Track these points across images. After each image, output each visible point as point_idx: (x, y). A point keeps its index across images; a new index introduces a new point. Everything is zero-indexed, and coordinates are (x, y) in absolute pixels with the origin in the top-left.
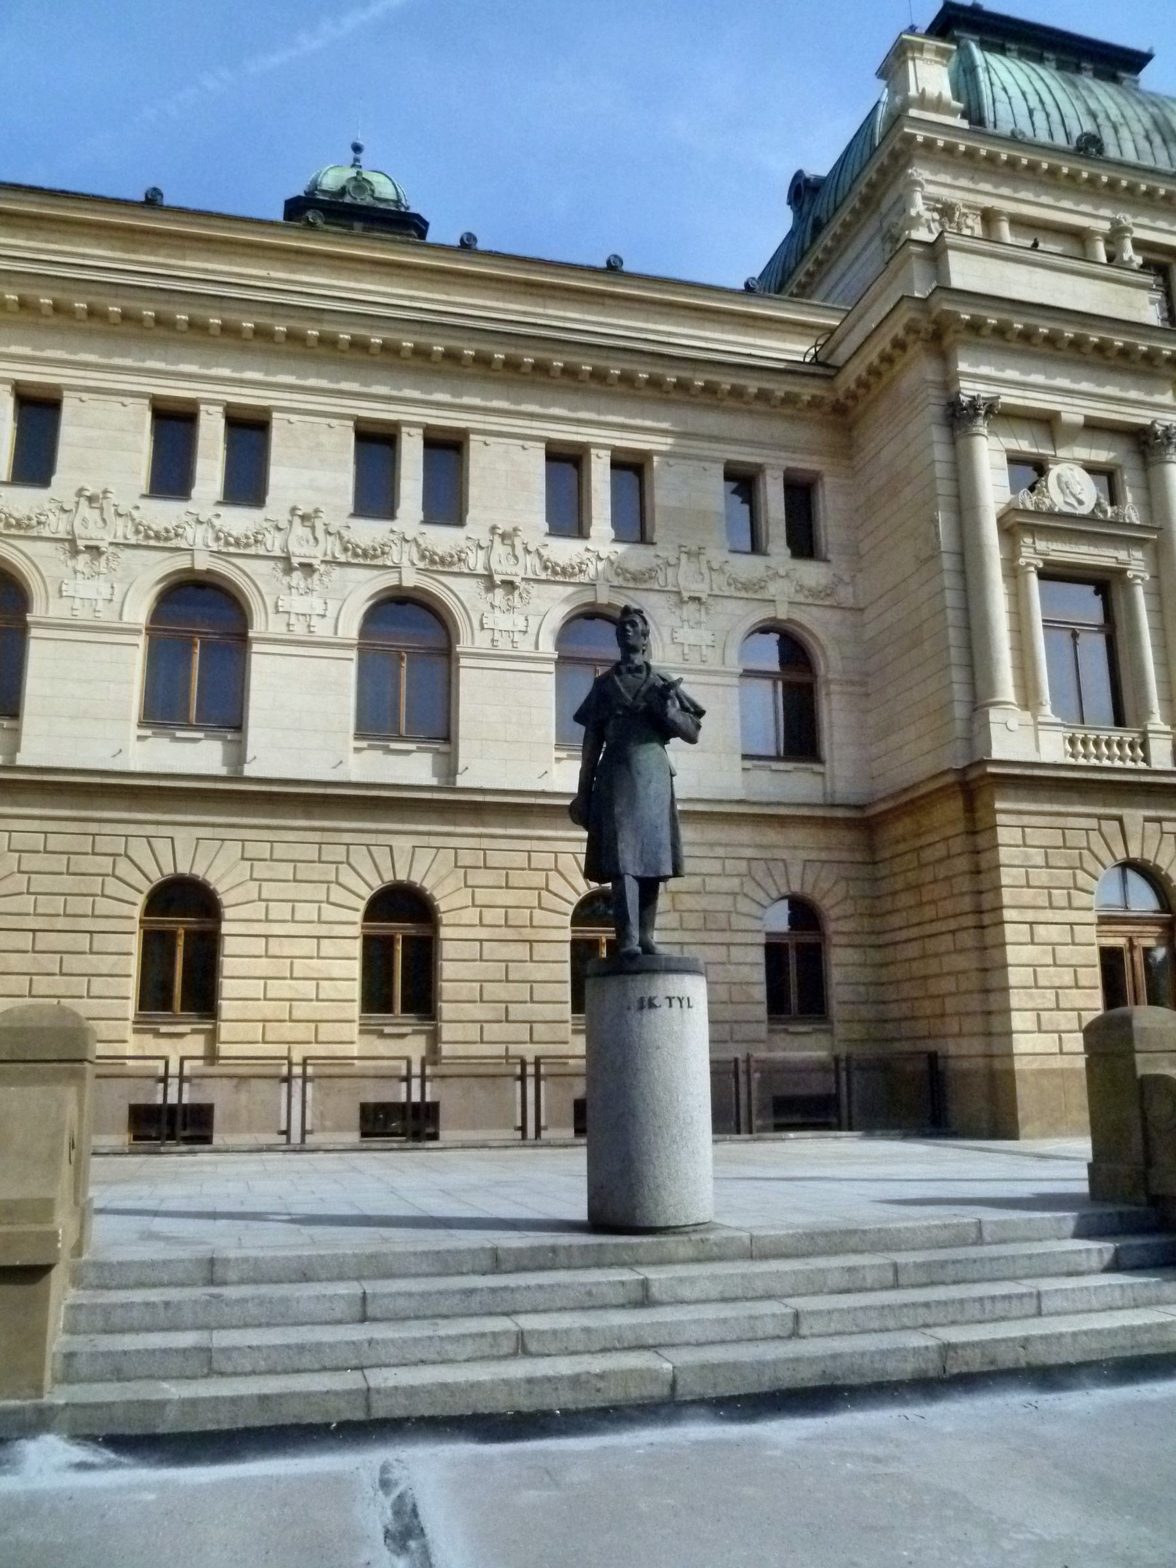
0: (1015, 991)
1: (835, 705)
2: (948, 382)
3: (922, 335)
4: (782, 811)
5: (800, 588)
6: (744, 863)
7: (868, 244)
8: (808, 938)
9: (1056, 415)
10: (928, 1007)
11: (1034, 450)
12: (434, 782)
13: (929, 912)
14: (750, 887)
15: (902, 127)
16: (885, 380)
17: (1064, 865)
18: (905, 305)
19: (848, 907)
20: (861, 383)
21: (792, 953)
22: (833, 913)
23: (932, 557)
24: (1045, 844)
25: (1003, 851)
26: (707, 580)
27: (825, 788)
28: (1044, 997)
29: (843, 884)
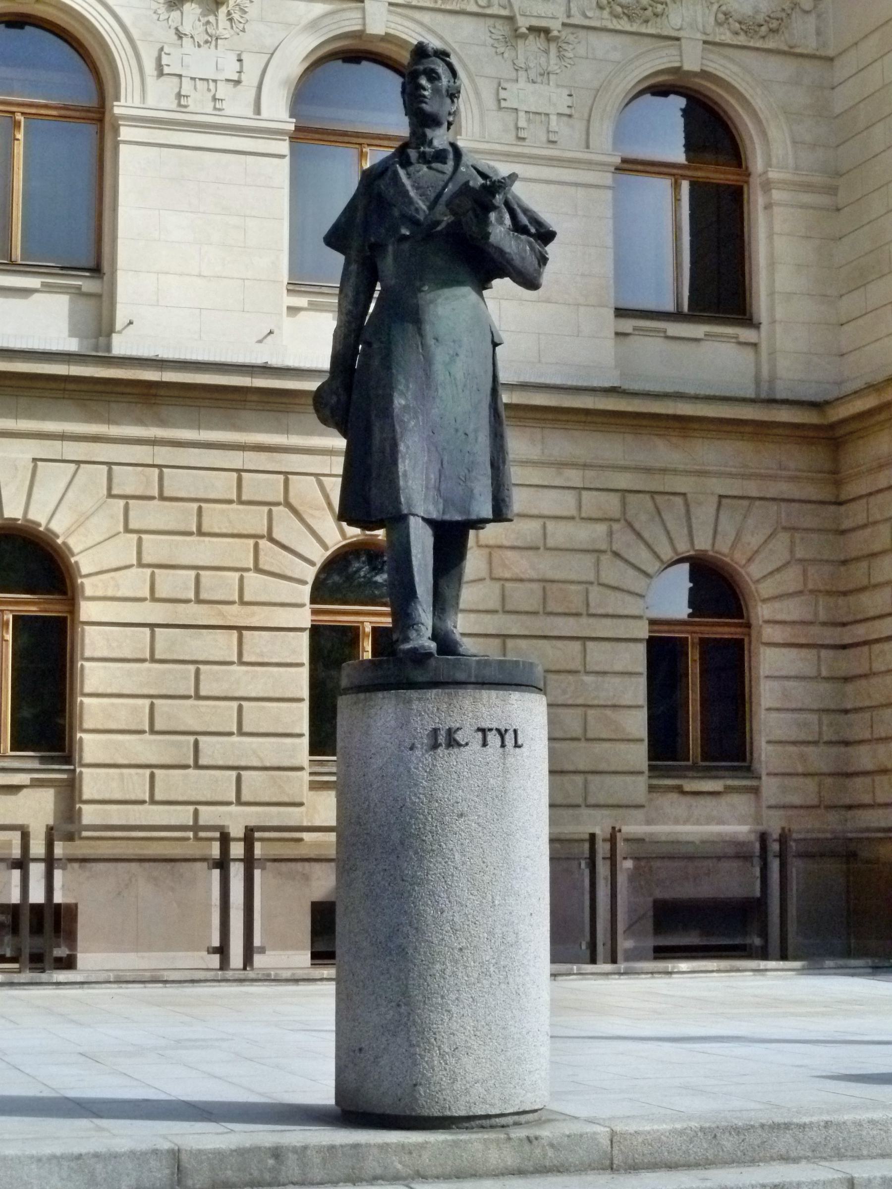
12: (72, 345)
14: (623, 540)
21: (693, 655)
29: (784, 538)
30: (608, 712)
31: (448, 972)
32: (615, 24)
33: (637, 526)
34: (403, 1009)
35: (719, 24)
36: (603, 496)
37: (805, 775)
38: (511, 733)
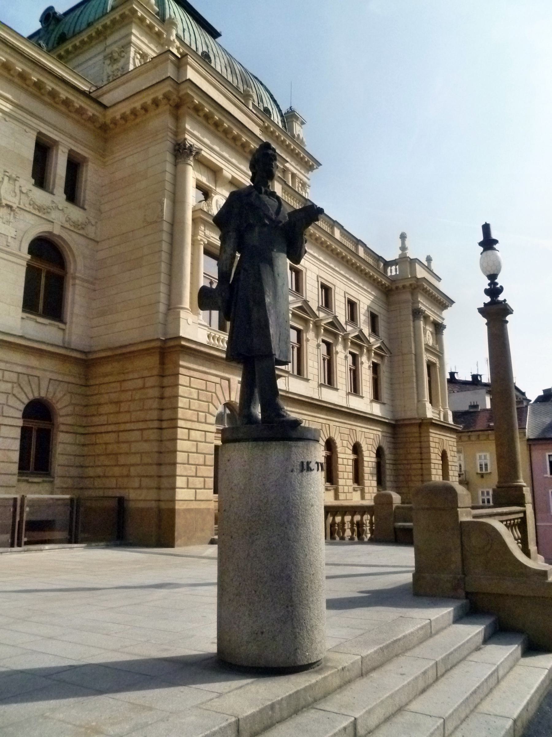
0: (179, 465)
1: (77, 292)
2: (179, 131)
3: (171, 102)
4: (44, 347)
5: (68, 220)
6: (15, 375)
7: (95, 56)
8: (43, 425)
9: (221, 170)
10: (117, 471)
11: (208, 184)
13: (127, 417)
14: (16, 391)
15: (132, 4)
16: (138, 120)
17: (205, 400)
18: (168, 82)
19: (69, 409)
20: (124, 117)
21: (34, 434)
22: (62, 412)
23: (156, 222)
24: (199, 388)
25: (181, 388)
26: (18, 197)
27: (64, 338)
28: (190, 470)
29: (69, 395)
30: (6, 452)
31: (309, 587)
32: (34, 211)
33: (22, 385)
34: (290, 609)
35: (67, 221)
36: (12, 374)
37: (68, 477)
38: (52, 479)
